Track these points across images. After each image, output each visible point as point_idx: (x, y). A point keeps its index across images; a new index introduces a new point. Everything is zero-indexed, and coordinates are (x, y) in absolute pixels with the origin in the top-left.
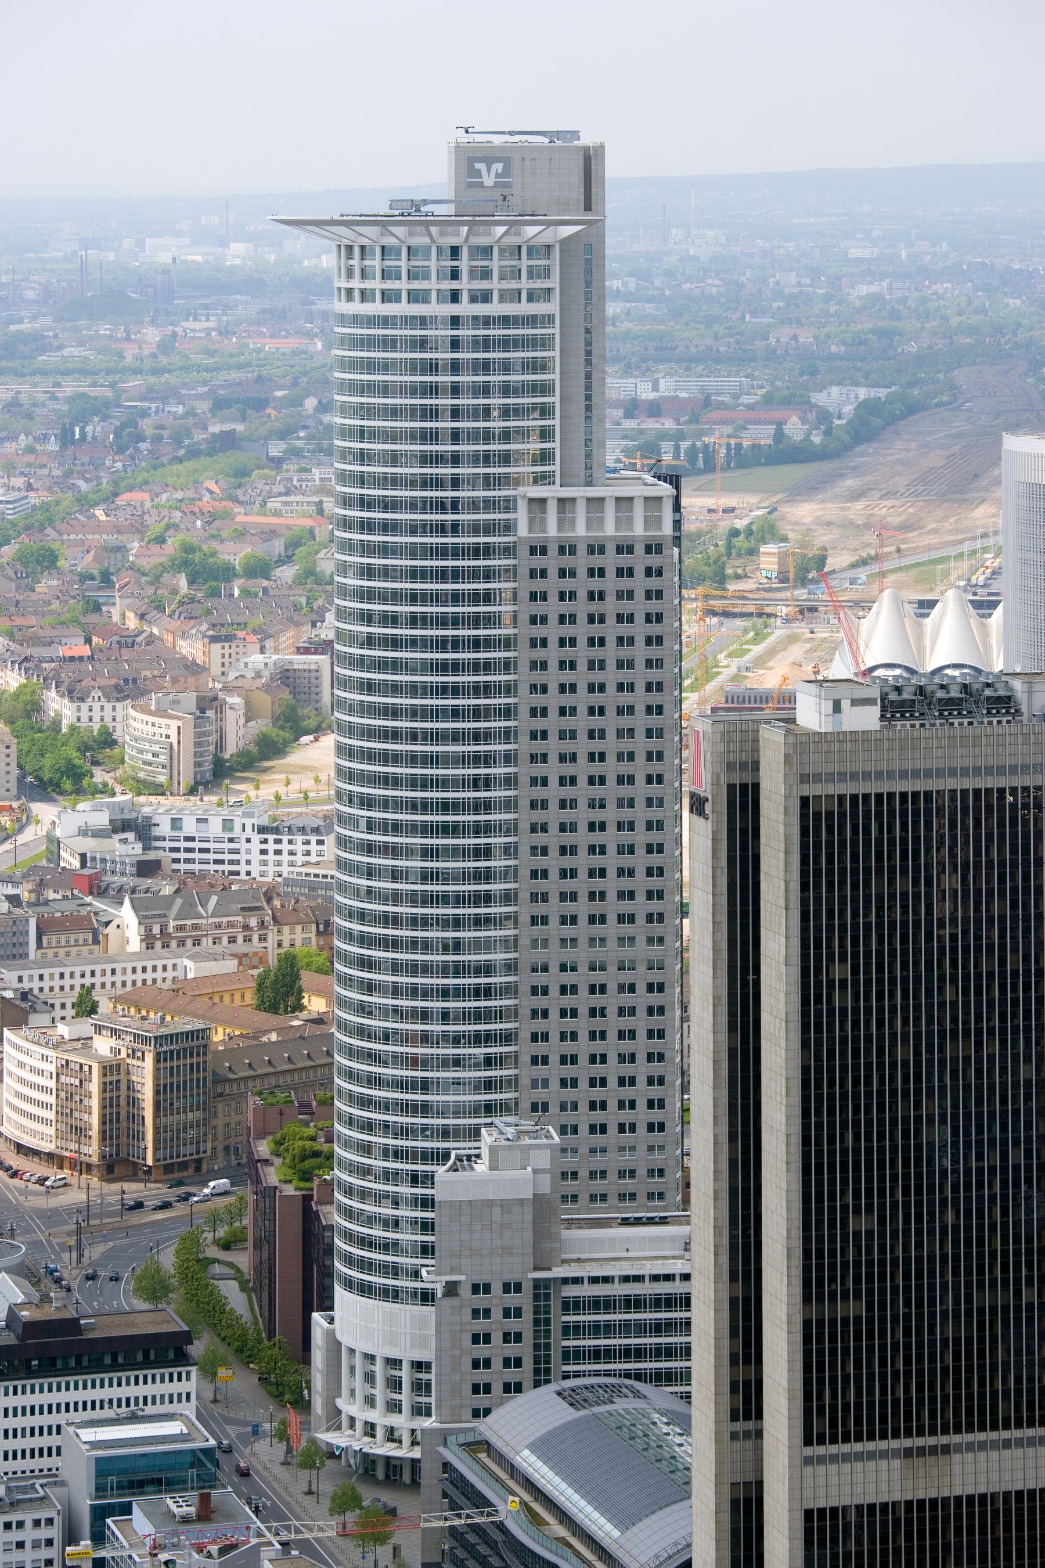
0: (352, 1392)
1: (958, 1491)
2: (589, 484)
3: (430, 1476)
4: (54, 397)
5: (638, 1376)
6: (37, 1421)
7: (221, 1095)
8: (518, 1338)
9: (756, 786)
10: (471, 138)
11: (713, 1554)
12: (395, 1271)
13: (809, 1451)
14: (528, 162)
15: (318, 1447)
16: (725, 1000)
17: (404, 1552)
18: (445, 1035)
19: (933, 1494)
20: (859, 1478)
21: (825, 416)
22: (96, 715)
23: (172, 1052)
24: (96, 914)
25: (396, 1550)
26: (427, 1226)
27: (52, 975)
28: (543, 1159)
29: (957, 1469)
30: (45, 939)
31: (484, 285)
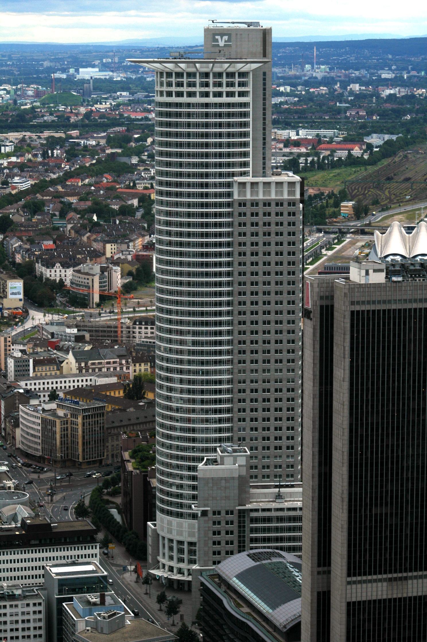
0: (164, 554)
1: (410, 595)
2: (264, 176)
3: (195, 588)
4: (39, 137)
5: (282, 548)
6: (34, 564)
7: (110, 433)
8: (232, 533)
9: (332, 306)
10: (215, 25)
11: (309, 619)
12: (181, 506)
13: (349, 579)
14: (239, 36)
15: (150, 576)
16: (318, 396)
17: (185, 617)
18: (202, 409)
19: (400, 596)
20: (369, 589)
21: (370, 146)
22: (58, 273)
23: (89, 415)
24: (58, 358)
25: (182, 617)
26: (194, 488)
27: (39, 383)
28: (242, 461)
29: (410, 586)
30: (36, 368)
31: (206, 89)
